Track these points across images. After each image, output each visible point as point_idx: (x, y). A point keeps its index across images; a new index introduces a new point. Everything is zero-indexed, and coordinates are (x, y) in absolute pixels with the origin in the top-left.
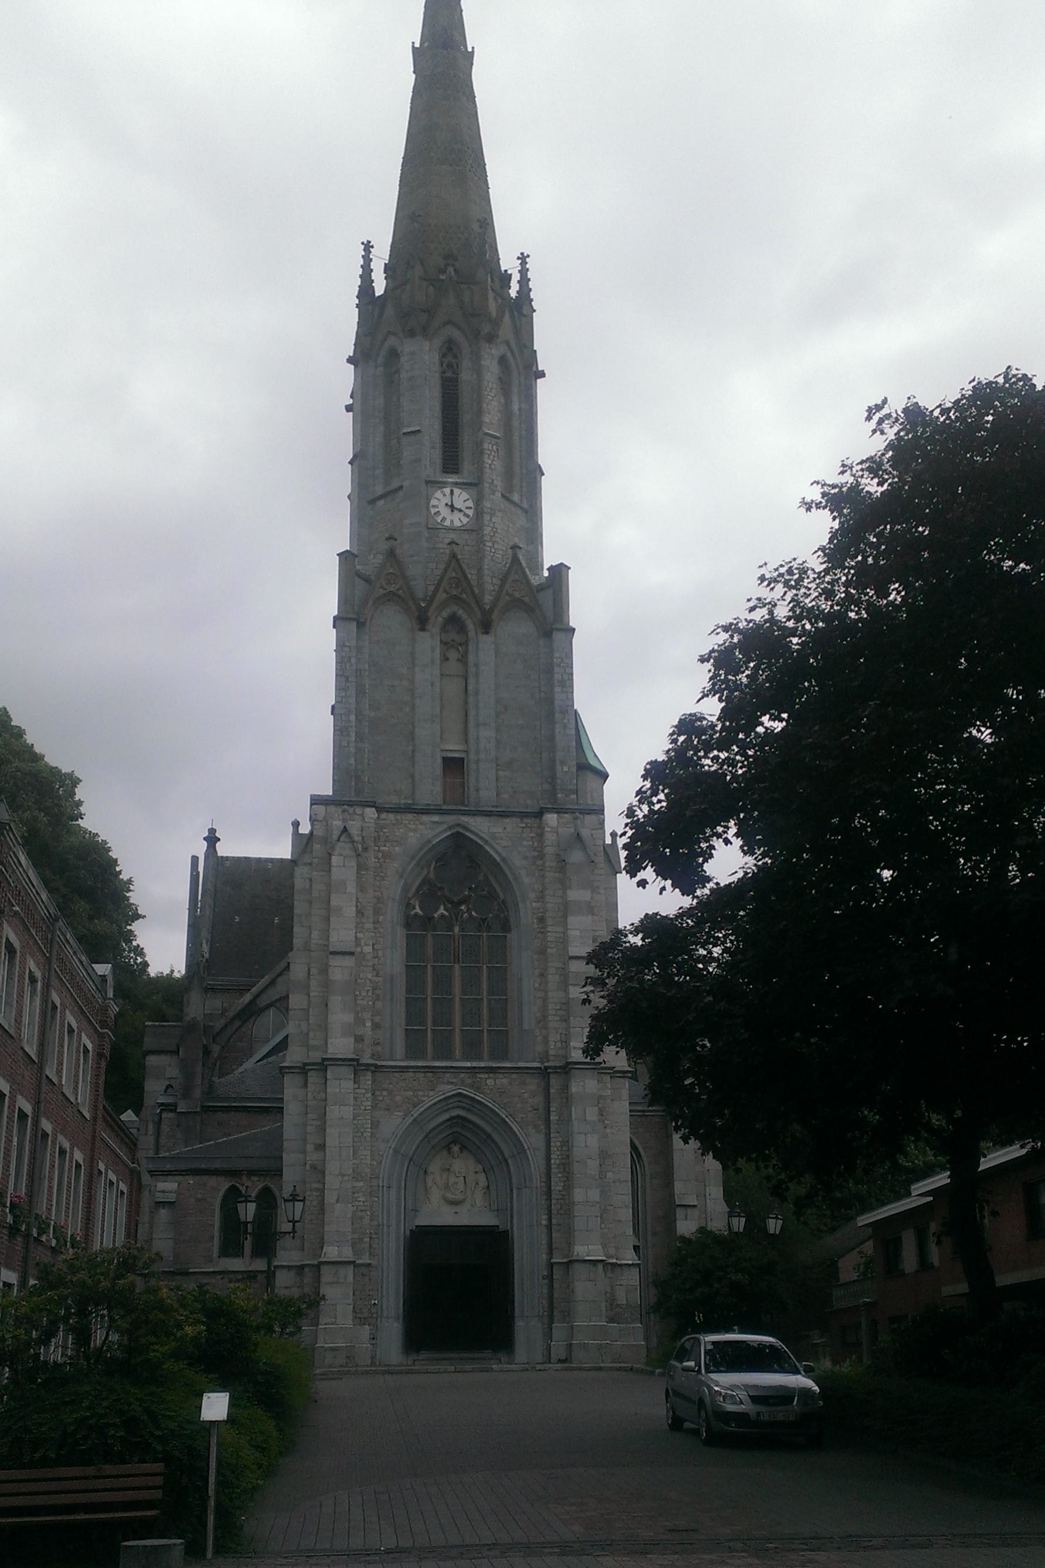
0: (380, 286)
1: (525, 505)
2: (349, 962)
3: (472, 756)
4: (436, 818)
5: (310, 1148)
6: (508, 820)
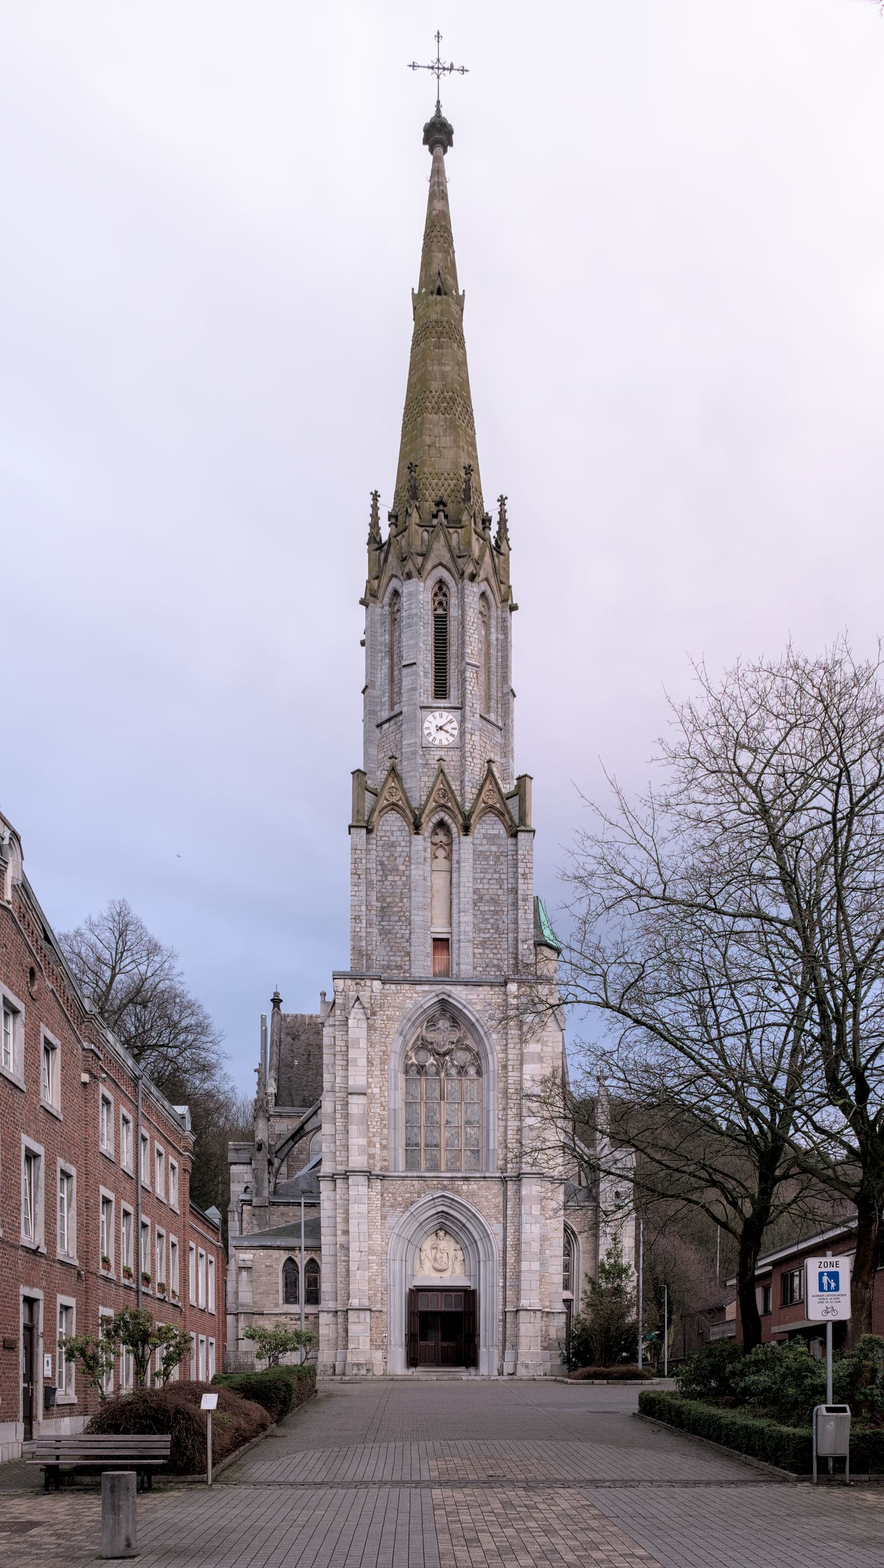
0: (385, 532)
1: (500, 724)
2: (362, 1100)
3: (455, 938)
4: (426, 988)
5: (339, 1233)
6: (480, 989)
